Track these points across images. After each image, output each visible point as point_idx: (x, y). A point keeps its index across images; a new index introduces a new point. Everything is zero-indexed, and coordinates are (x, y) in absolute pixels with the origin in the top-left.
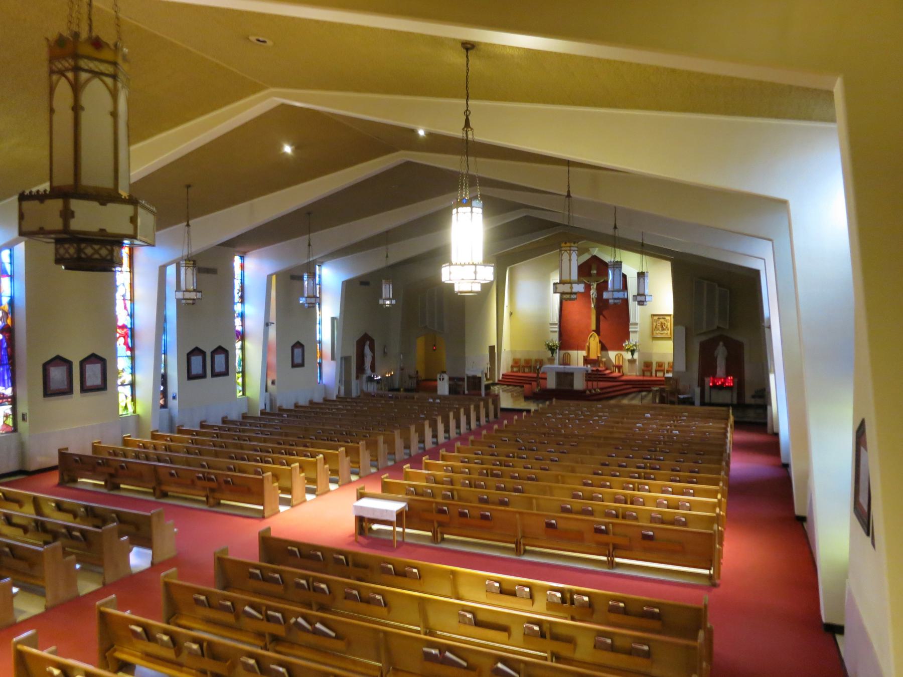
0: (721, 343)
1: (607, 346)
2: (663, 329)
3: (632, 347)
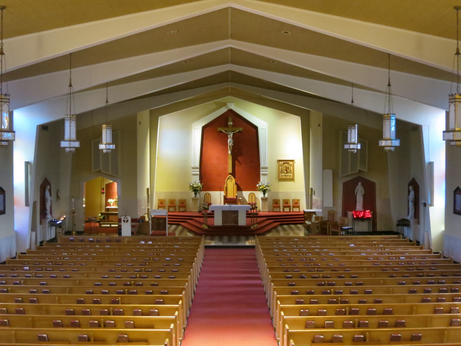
0: (360, 184)
1: (241, 186)
2: (287, 173)
3: (265, 187)
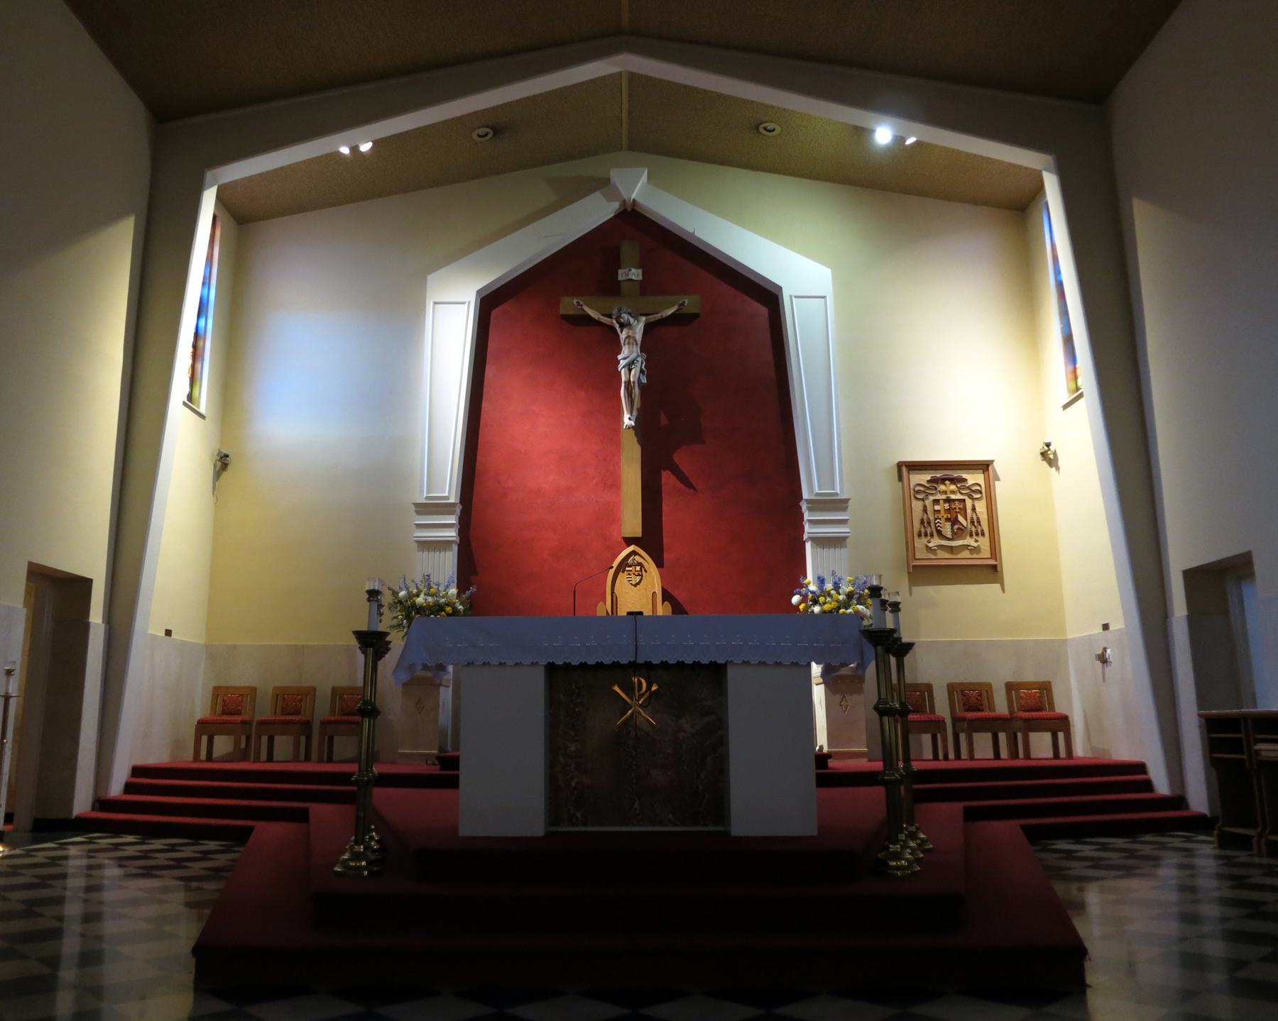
2: (959, 532)
